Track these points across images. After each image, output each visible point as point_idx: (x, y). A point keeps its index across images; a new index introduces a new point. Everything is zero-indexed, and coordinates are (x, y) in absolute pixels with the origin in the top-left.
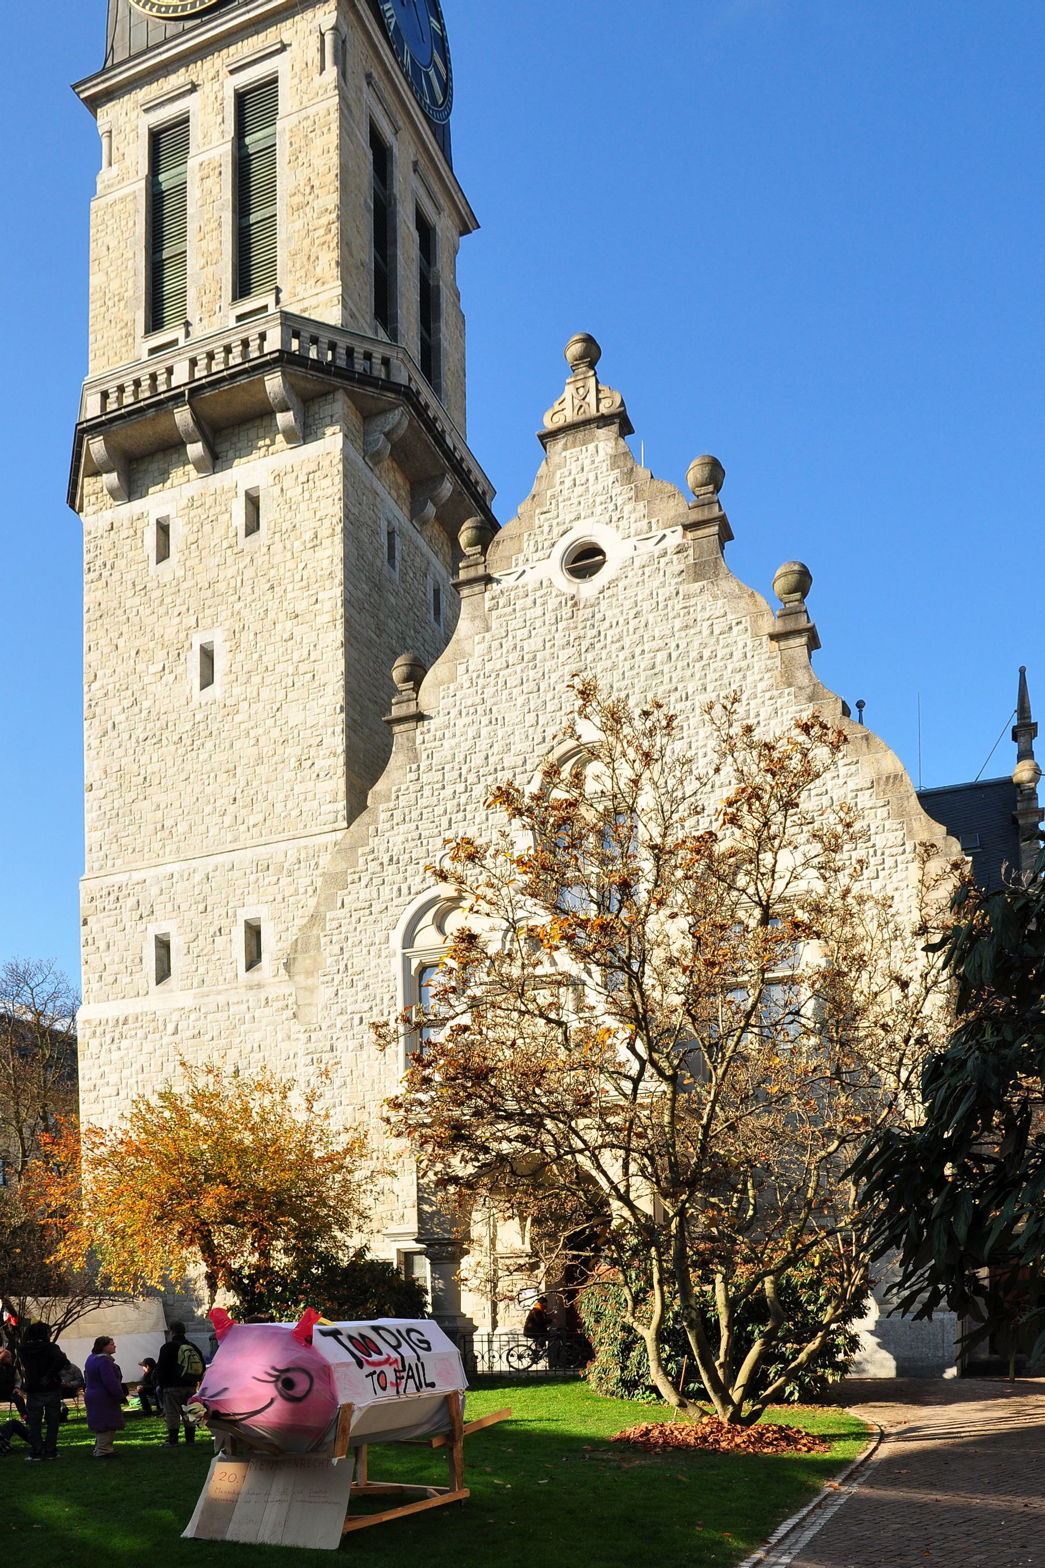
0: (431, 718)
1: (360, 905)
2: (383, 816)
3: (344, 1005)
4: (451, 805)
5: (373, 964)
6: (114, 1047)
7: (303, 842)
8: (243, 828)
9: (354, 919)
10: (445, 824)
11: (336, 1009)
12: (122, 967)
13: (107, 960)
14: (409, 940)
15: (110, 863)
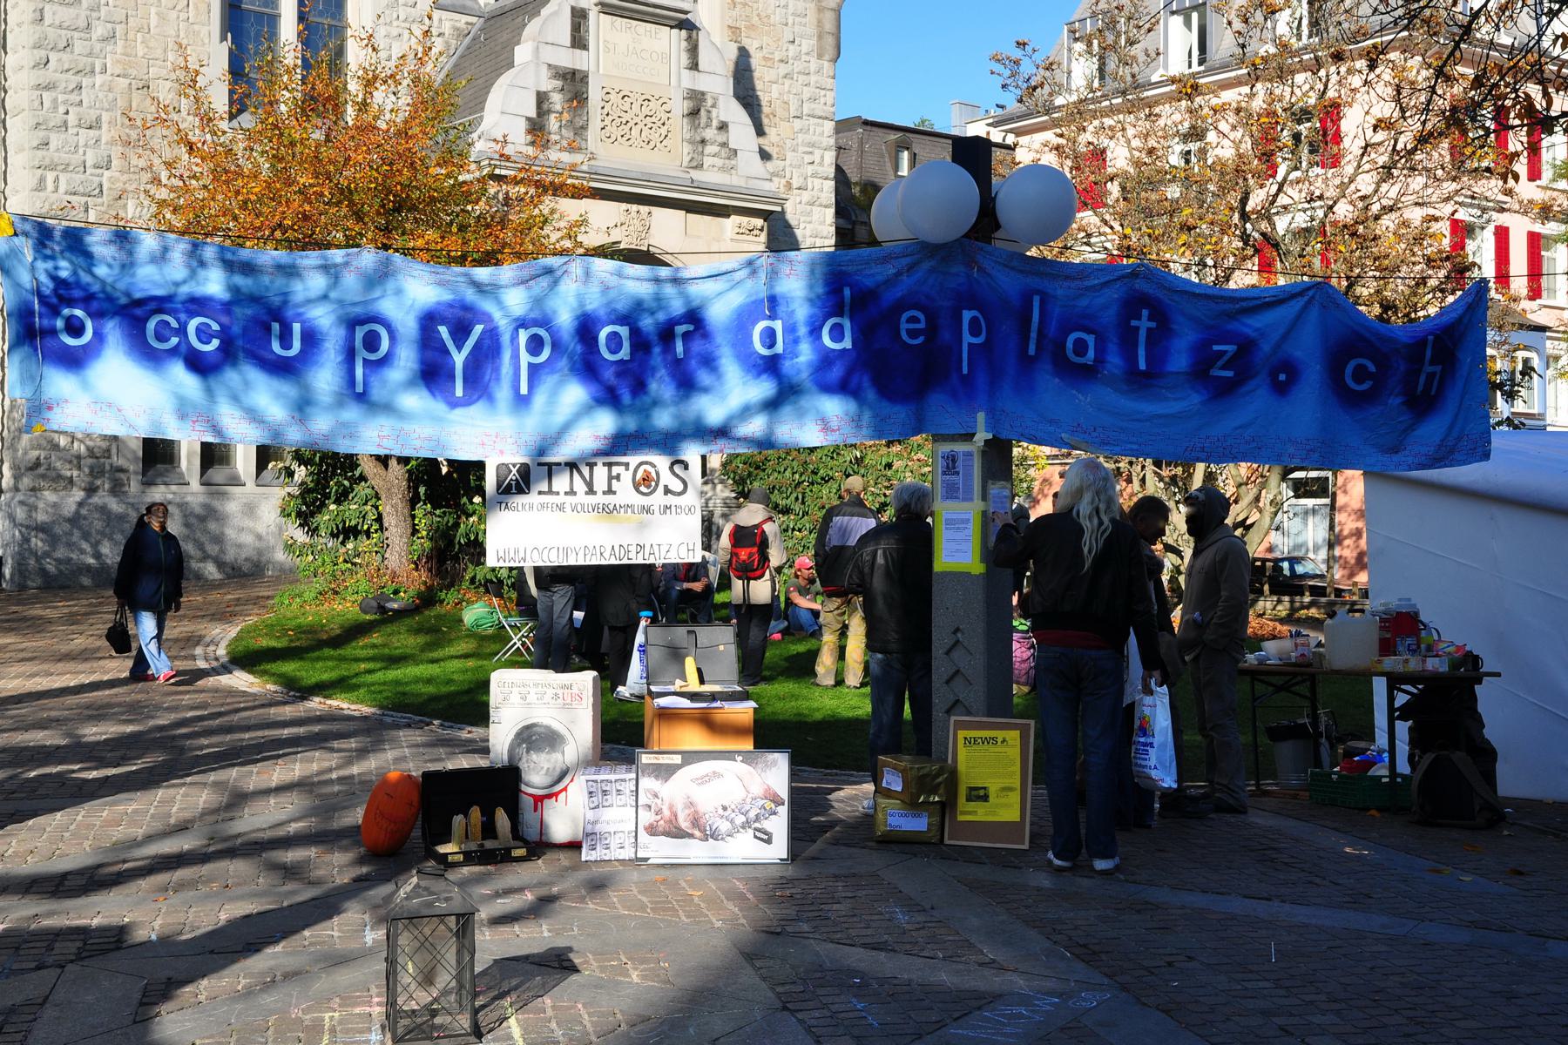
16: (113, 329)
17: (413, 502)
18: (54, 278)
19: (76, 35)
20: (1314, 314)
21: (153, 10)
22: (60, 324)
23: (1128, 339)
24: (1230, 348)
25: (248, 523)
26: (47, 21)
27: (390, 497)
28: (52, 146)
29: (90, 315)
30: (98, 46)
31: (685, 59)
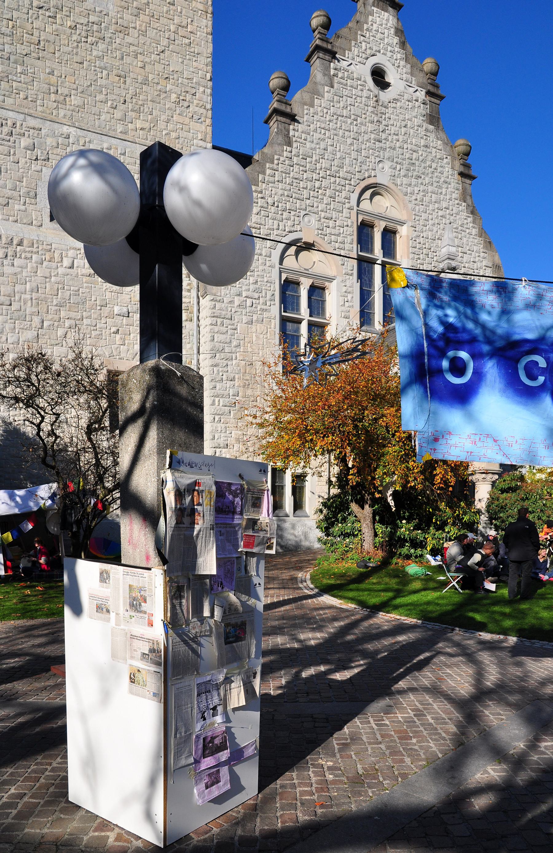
0: (299, 123)
2: (268, 172)
3: (240, 289)
5: (261, 268)
10: (305, 193)
16: (491, 369)
17: (374, 521)
18: (443, 322)
19: (226, 345)
21: (254, 334)
22: (445, 364)
25: (292, 531)
26: (215, 340)
27: (365, 520)
28: (217, 388)
29: (474, 356)
30: (234, 349)
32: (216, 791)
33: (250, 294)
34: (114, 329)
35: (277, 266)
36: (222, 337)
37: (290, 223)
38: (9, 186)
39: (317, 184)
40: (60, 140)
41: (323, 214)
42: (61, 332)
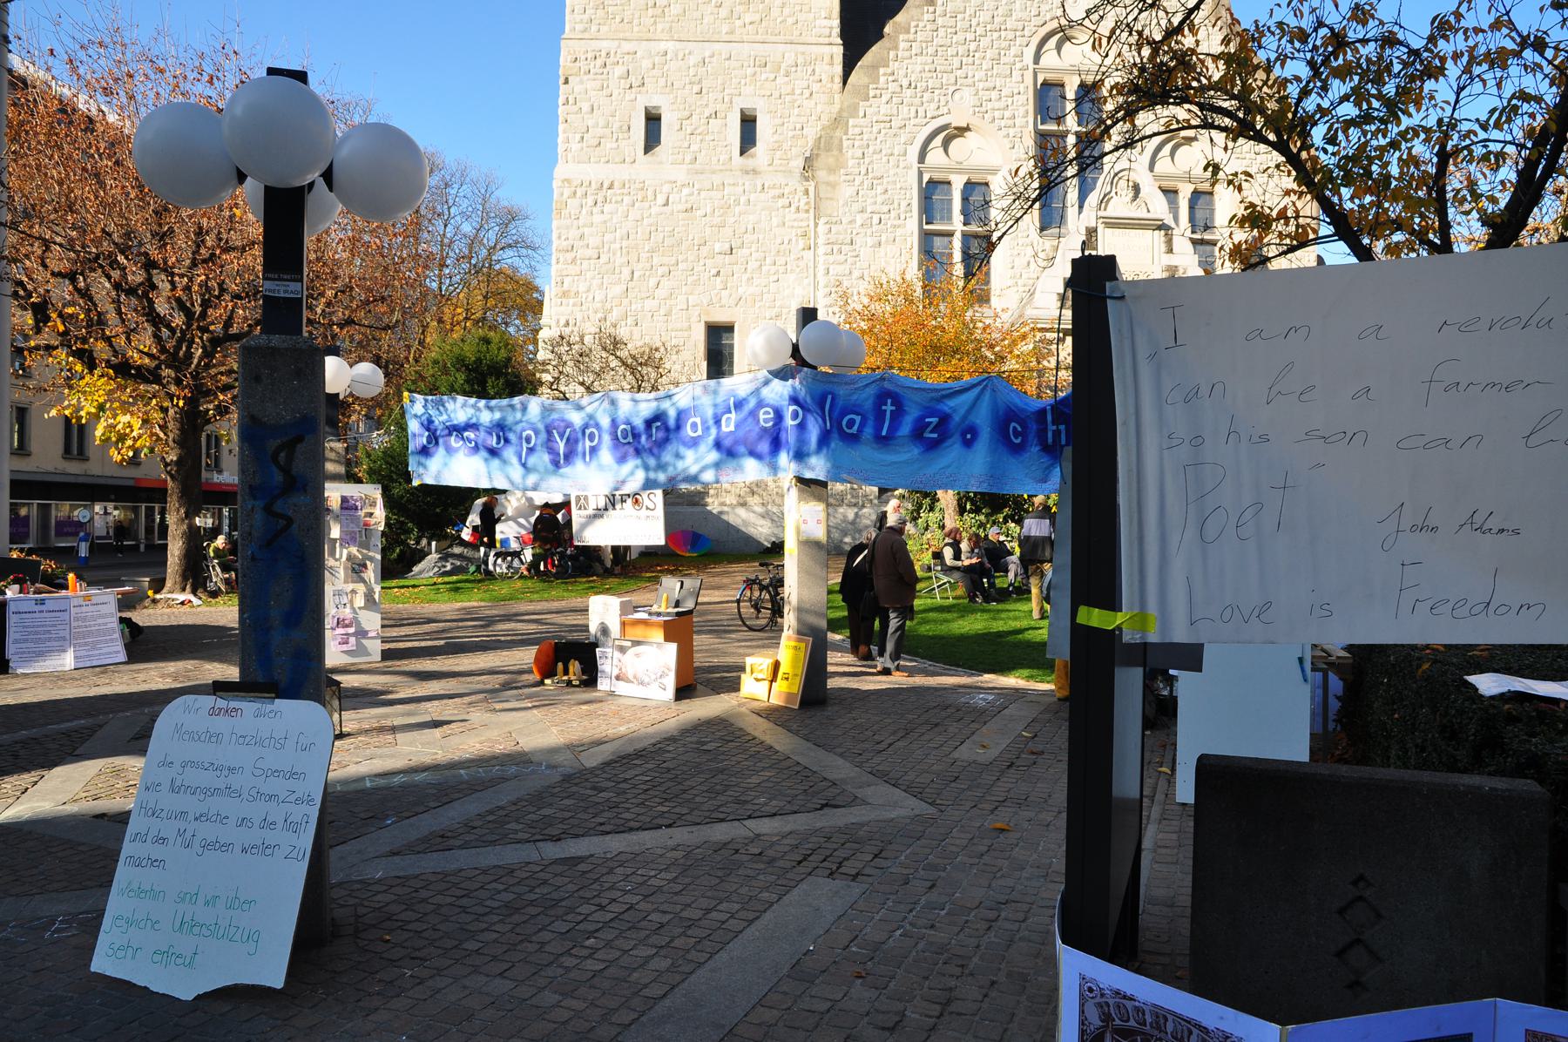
1: (882, 118)
2: (902, 45)
4: (961, 50)
5: (891, 172)
6: (595, 210)
7: (801, 48)
8: (738, 23)
9: (875, 129)
10: (956, 64)
11: (856, 207)
12: (608, 131)
13: (590, 123)
14: (922, 157)
15: (594, 28)
20: (987, 396)
23: (880, 416)
24: (934, 420)
31: (1163, 248)
32: (345, 647)
33: (876, 208)
34: (714, 271)
35: (916, 165)
36: (840, 269)
37: (933, 106)
38: (602, 123)
39: (973, 46)
40: (657, 60)
41: (981, 85)
42: (653, 282)
